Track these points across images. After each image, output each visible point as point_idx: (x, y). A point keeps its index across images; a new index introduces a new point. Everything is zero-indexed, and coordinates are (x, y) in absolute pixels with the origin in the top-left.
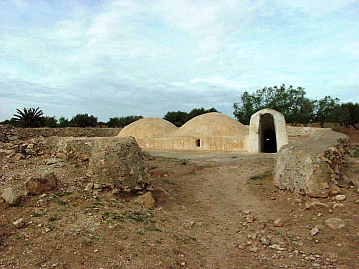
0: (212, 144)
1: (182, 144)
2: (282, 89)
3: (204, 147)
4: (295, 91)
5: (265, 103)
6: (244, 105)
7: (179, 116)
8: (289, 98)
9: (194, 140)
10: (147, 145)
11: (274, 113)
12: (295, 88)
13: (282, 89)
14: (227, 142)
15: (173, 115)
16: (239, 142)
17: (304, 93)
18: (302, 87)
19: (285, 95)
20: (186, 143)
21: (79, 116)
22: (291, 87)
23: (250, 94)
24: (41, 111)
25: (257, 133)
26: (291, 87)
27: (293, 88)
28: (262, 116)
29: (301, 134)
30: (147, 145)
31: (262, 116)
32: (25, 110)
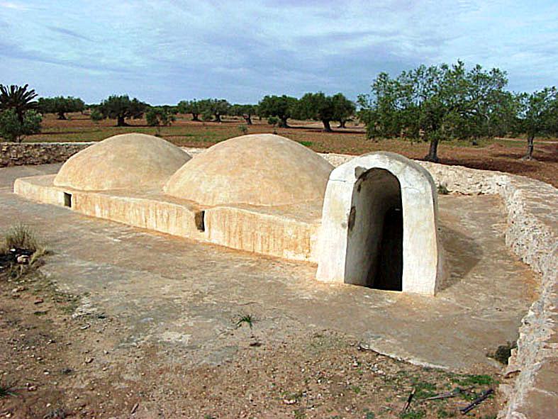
0: (233, 230)
1: (165, 221)
2: (459, 71)
3: (214, 234)
4: (484, 77)
5: (420, 99)
6: (379, 98)
7: (284, 104)
8: (471, 91)
9: (192, 214)
10: (98, 210)
11: (403, 170)
12: (487, 69)
13: (459, 71)
14: (268, 230)
15: (273, 101)
16: (300, 238)
17: (503, 82)
18: (502, 71)
19: (464, 84)
20: (173, 219)
21: (114, 98)
22: (478, 67)
23: (392, 77)
24: (33, 91)
25: (343, 226)
26: (478, 67)
27: (482, 71)
28: (364, 176)
29: (485, 190)
30: (98, 210)
31: (364, 176)
32: (13, 88)
